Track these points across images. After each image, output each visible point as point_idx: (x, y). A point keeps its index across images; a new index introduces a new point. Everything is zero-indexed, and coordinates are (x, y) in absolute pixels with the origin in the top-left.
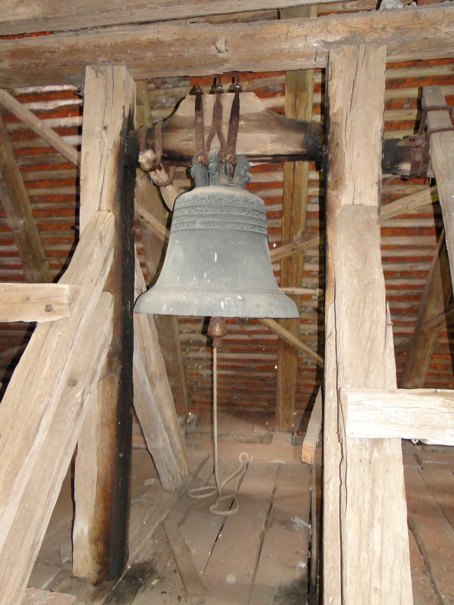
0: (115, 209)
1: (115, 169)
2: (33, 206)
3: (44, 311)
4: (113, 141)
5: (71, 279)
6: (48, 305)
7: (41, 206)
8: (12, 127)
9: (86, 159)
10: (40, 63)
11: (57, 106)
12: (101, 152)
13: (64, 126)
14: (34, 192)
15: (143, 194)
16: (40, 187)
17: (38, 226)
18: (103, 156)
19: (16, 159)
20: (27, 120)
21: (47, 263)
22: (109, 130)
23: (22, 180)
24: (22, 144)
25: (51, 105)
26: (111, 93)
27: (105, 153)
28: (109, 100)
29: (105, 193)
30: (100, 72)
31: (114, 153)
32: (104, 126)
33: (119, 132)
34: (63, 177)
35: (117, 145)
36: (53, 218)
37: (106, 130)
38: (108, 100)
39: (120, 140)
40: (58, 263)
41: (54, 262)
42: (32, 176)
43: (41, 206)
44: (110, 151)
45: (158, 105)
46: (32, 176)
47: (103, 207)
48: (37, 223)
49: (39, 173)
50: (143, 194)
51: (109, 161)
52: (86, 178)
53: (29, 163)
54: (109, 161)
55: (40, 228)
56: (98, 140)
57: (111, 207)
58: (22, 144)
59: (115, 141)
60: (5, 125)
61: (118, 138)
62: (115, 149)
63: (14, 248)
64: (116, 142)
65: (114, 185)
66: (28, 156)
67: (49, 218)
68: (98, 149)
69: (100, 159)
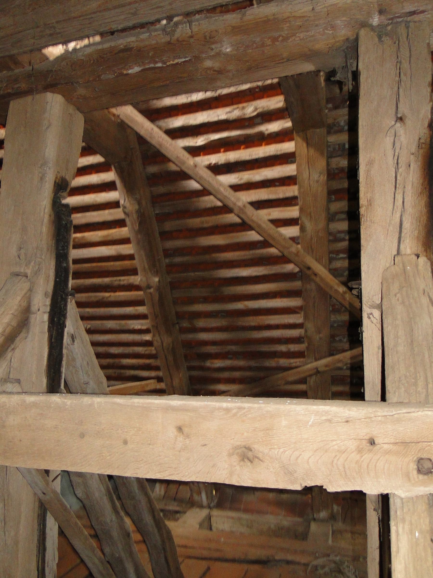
0: (428, 251)
1: (422, 185)
2: (167, 261)
3: (415, 472)
4: (417, 138)
5: (419, 389)
6: (422, 459)
7: (178, 260)
8: (153, 169)
9: (368, 172)
10: (280, 36)
11: (209, 140)
12: (396, 158)
13: (215, 164)
14: (171, 244)
15: (312, 238)
16: (178, 238)
17: (171, 283)
18: (400, 165)
19: (153, 207)
20: (177, 157)
21: (177, 326)
22: (408, 122)
23: (158, 231)
24: (161, 190)
25: (200, 141)
26: (408, 63)
27: (403, 161)
28: (405, 75)
29: (407, 225)
30: (387, 34)
31: (420, 158)
32: (399, 116)
33: (426, 125)
34: (205, 225)
35: (423, 146)
36: (190, 274)
37: (404, 124)
38: (402, 74)
39: (428, 136)
40: (190, 326)
41: (185, 325)
42: (169, 226)
43: (178, 260)
44: (412, 157)
45: (336, 128)
46: (169, 226)
47: (406, 248)
48: (170, 280)
49: (178, 222)
50: (312, 238)
51: (411, 172)
52: (370, 203)
53: (167, 211)
54: (411, 172)
55: (173, 286)
56: (389, 140)
57: (420, 249)
58: (161, 190)
59: (420, 139)
60: (145, 168)
61: (425, 133)
62: (421, 151)
63: (141, 309)
64: (422, 141)
65: (424, 210)
66: (167, 203)
67: (185, 274)
68: (390, 153)
69: (394, 170)
